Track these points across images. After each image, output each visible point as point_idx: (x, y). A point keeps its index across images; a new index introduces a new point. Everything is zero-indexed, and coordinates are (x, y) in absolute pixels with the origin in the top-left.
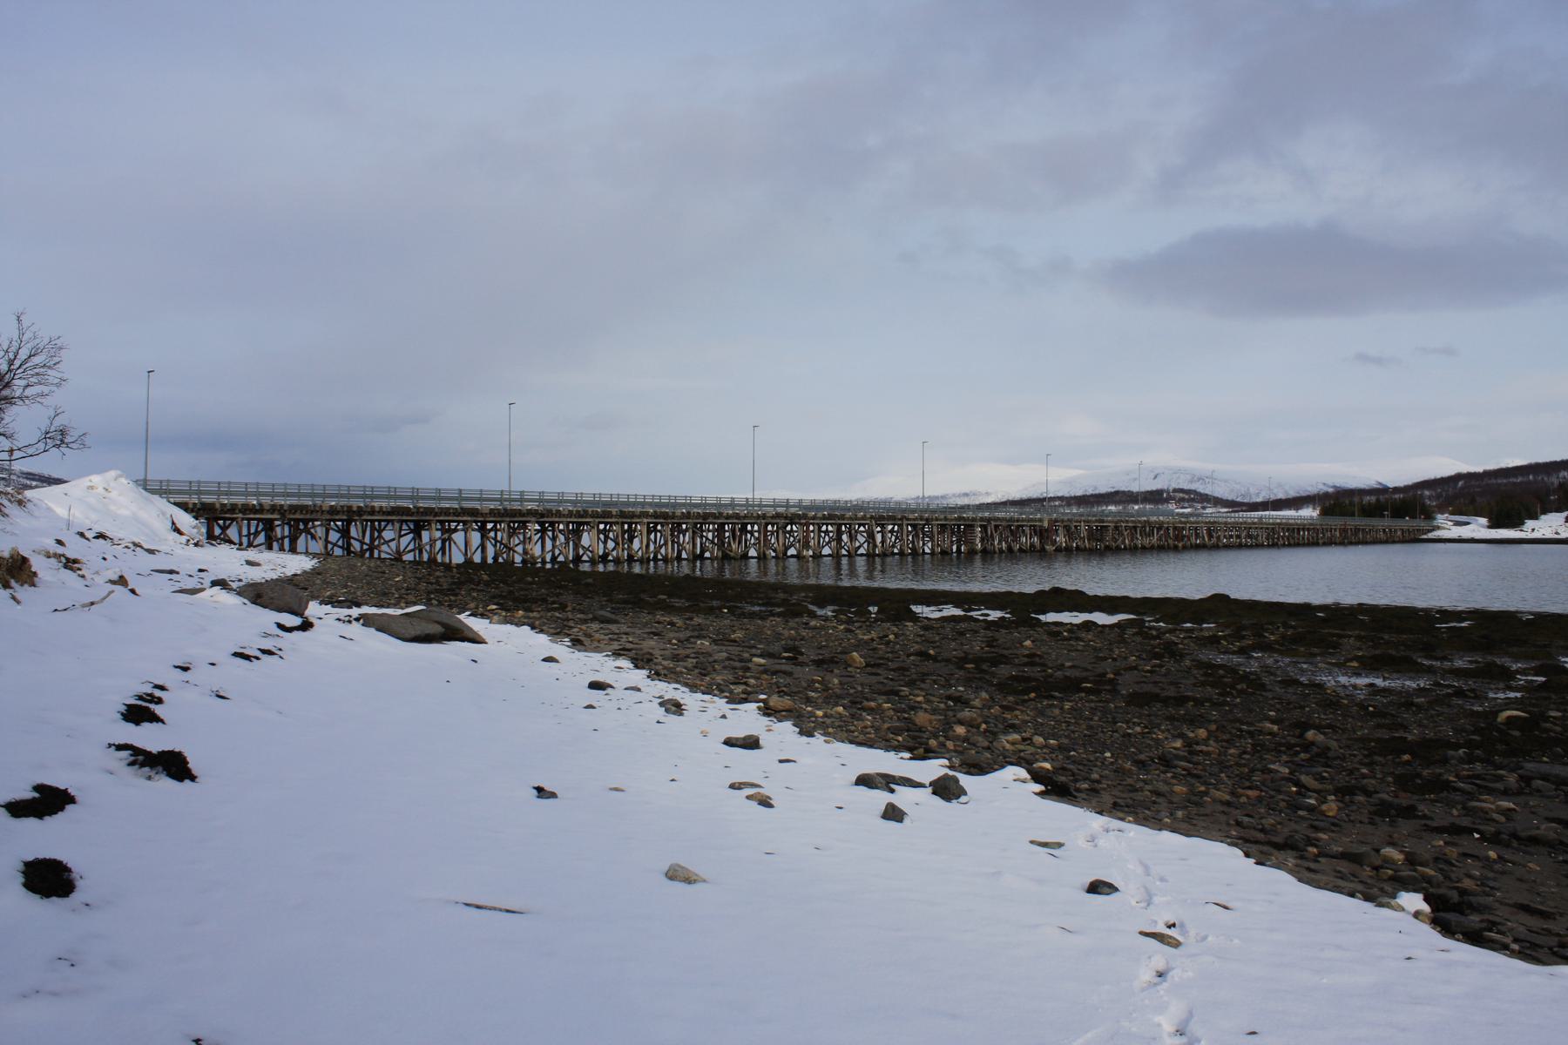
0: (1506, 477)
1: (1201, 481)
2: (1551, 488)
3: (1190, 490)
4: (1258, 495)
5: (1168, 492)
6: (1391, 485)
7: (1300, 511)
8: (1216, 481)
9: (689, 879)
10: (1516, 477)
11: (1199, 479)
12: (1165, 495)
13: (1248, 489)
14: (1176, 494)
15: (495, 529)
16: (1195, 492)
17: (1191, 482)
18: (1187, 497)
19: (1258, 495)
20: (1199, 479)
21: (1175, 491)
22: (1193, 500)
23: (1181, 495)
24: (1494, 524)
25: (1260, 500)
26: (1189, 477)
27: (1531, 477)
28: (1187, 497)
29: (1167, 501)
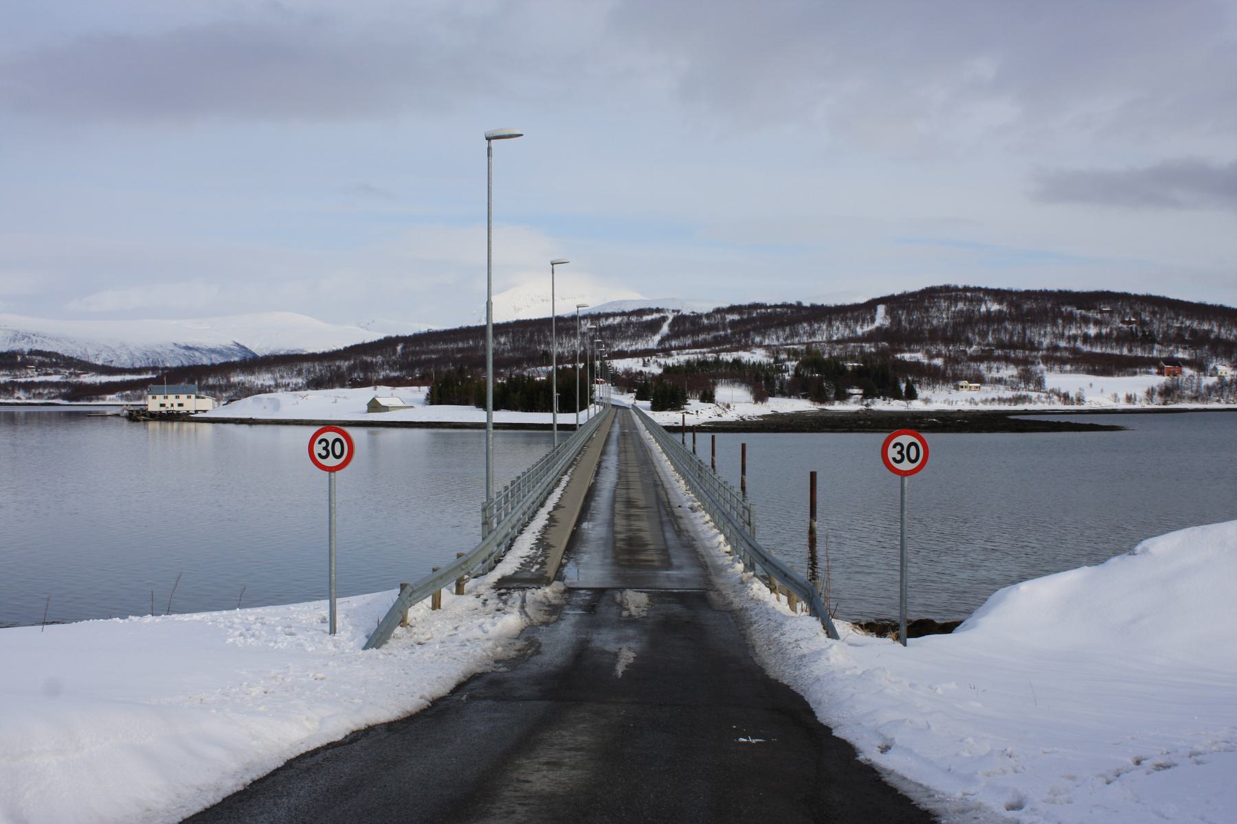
0: (445, 342)
1: (26, 340)
2: (1033, 301)
3: (50, 353)
4: (97, 356)
5: (22, 354)
6: (441, 689)
7: (687, 358)
8: (45, 340)
9: (436, 570)
10: (456, 341)
11: (24, 337)
12: (19, 359)
13: (85, 349)
14: (34, 357)
15: (641, 380)
16: (56, 355)
17: (14, 340)
18: (47, 360)
19: (97, 356)
20: (24, 337)
21: (31, 353)
22: (56, 365)
23: (40, 358)
24: (436, 398)
25: (100, 362)
26: (10, 335)
27: (471, 343)
28: (47, 360)
29: (24, 365)
